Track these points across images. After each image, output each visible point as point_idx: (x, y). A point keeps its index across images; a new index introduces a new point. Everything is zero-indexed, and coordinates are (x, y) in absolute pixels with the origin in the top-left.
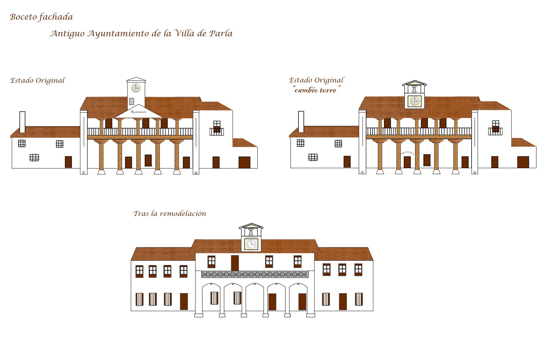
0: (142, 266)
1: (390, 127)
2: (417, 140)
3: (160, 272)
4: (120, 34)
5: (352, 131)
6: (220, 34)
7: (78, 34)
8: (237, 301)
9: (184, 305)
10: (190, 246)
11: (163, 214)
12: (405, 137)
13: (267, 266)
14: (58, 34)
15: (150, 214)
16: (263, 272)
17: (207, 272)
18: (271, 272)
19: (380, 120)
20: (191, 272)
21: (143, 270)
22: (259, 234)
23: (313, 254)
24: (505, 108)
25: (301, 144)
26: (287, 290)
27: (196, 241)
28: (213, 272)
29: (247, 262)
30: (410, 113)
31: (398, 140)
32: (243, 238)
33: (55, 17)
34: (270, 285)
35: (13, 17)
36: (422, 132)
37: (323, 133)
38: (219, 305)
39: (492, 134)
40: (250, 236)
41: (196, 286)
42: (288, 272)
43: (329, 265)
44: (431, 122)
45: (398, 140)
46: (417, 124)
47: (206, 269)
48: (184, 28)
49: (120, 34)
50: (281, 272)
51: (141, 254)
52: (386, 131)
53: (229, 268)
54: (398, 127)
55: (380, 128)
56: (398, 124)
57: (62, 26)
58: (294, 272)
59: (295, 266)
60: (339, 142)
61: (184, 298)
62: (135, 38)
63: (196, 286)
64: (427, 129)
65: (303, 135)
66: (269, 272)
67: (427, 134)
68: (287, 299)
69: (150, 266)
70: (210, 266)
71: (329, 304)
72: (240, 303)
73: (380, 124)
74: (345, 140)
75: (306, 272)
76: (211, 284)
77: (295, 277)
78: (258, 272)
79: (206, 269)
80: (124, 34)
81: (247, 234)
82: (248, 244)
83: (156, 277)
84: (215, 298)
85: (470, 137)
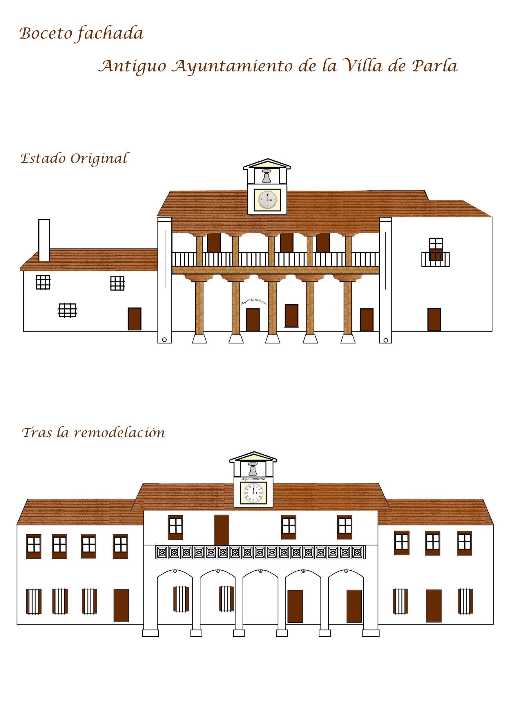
0: (39, 536)
1: (219, 251)
2: (271, 276)
3: (74, 548)
4: (236, 67)
5: (144, 259)
6: (434, 67)
7: (153, 68)
8: (181, 604)
9: (121, 614)
10: (134, 497)
11: (79, 434)
12: (247, 270)
13: (285, 536)
14: (113, 68)
15: (54, 434)
16: (276, 547)
17: (166, 547)
18: (292, 547)
19: (199, 237)
20: (134, 548)
21: (66, 544)
22: (269, 474)
23: (376, 512)
24: (490, 216)
25: (43, 284)
26: (325, 584)
27: (145, 487)
28: (179, 547)
29: (244, 528)
30: (259, 224)
31: (235, 275)
32: (238, 481)
33: (107, 33)
34: (290, 573)
35: (26, 33)
36: (283, 260)
37: (87, 262)
38: (189, 613)
39: (428, 264)
40: (250, 476)
41: (145, 575)
42: (325, 547)
43: (407, 533)
44: (300, 242)
45: (235, 275)
46: (271, 244)
47: (164, 541)
48: (362, 57)
49: (236, 67)
50: (252, 547)
51: (37, 511)
52: (212, 259)
53: (210, 540)
54: (235, 251)
55: (198, 252)
56: (235, 244)
57: (123, 50)
58: (337, 547)
59: (341, 536)
60: (118, 279)
61: (121, 598)
62: (266, 75)
63: (145, 575)
64: (292, 255)
65: (49, 266)
66: (288, 547)
67: (292, 264)
68: (325, 602)
69: (54, 536)
70: (172, 536)
71: (471, 612)
72: (232, 609)
73: (199, 244)
74: (130, 276)
75: (361, 547)
76: (218, 571)
77: (340, 557)
78: (267, 547)
79: (164, 541)
80: (244, 66)
81: (245, 473)
82: (248, 493)
83: (126, 557)
84: (182, 599)
85: (375, 270)
